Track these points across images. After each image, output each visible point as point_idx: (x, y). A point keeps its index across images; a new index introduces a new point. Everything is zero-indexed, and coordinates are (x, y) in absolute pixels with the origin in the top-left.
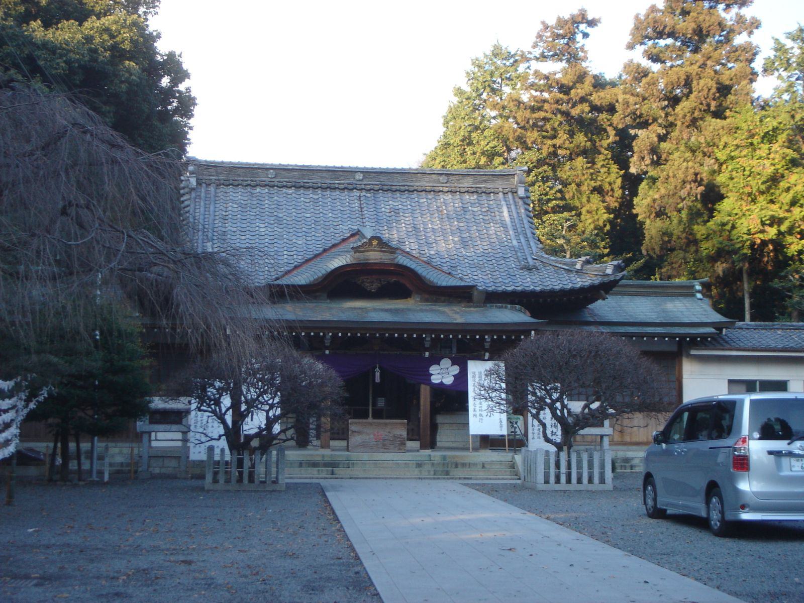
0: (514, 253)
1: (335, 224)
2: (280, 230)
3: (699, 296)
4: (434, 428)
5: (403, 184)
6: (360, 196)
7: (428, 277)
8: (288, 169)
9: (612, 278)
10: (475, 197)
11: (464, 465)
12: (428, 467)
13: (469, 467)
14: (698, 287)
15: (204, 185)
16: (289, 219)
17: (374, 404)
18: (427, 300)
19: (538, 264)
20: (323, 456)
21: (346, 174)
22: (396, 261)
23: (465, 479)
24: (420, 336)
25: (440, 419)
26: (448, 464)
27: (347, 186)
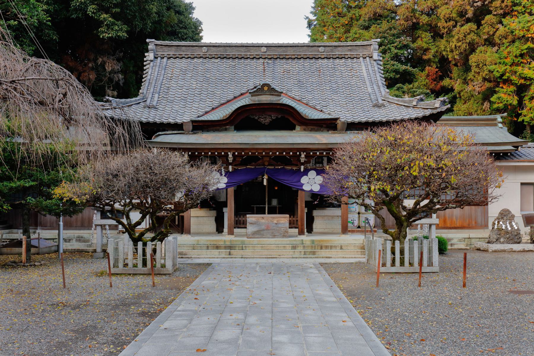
0: (368, 96)
1: (245, 80)
2: (206, 85)
3: (500, 125)
5: (294, 53)
6: (264, 63)
7: (304, 113)
8: (216, 46)
9: (439, 110)
10: (343, 61)
11: (327, 247)
12: (300, 249)
14: (500, 120)
15: (159, 58)
16: (213, 78)
17: (270, 203)
18: (305, 130)
19: (385, 103)
20: (225, 241)
21: (255, 48)
22: (281, 102)
23: (327, 257)
25: (315, 213)
26: (315, 246)
27: (255, 56)
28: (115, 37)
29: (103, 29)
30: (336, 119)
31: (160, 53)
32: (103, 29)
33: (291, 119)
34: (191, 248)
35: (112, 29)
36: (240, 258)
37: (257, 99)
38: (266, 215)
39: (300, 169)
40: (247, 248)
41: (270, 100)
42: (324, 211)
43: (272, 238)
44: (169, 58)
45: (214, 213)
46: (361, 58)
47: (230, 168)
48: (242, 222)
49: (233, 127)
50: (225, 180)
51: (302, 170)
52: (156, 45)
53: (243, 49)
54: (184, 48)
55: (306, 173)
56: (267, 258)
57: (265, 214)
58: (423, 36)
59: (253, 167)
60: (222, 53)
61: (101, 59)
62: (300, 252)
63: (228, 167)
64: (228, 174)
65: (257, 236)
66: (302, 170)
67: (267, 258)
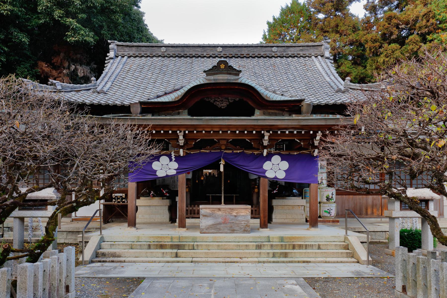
4: (271, 209)
11: (300, 247)
13: (306, 249)
15: (120, 57)
21: (211, 48)
22: (239, 81)
24: (259, 133)
25: (275, 202)
28: (82, 41)
29: (69, 34)
30: (301, 101)
31: (120, 53)
32: (69, 34)
33: (250, 103)
34: (128, 247)
35: (79, 34)
36: (189, 262)
37: (213, 79)
38: (223, 206)
39: (262, 154)
40: (200, 248)
41: (228, 79)
42: (284, 200)
43: (231, 233)
44: (129, 57)
45: (167, 202)
46: (313, 57)
47: (181, 152)
48: (196, 211)
49: (186, 111)
50: (175, 165)
51: (265, 154)
52: (118, 45)
53: (199, 49)
54: (143, 48)
55: (269, 157)
56: (225, 262)
57: (220, 203)
58: (345, 63)
59: (208, 151)
60: (180, 53)
61: (73, 67)
62: (268, 253)
63: (179, 151)
64: (178, 159)
65: (213, 231)
66: (265, 154)
67: (225, 262)
